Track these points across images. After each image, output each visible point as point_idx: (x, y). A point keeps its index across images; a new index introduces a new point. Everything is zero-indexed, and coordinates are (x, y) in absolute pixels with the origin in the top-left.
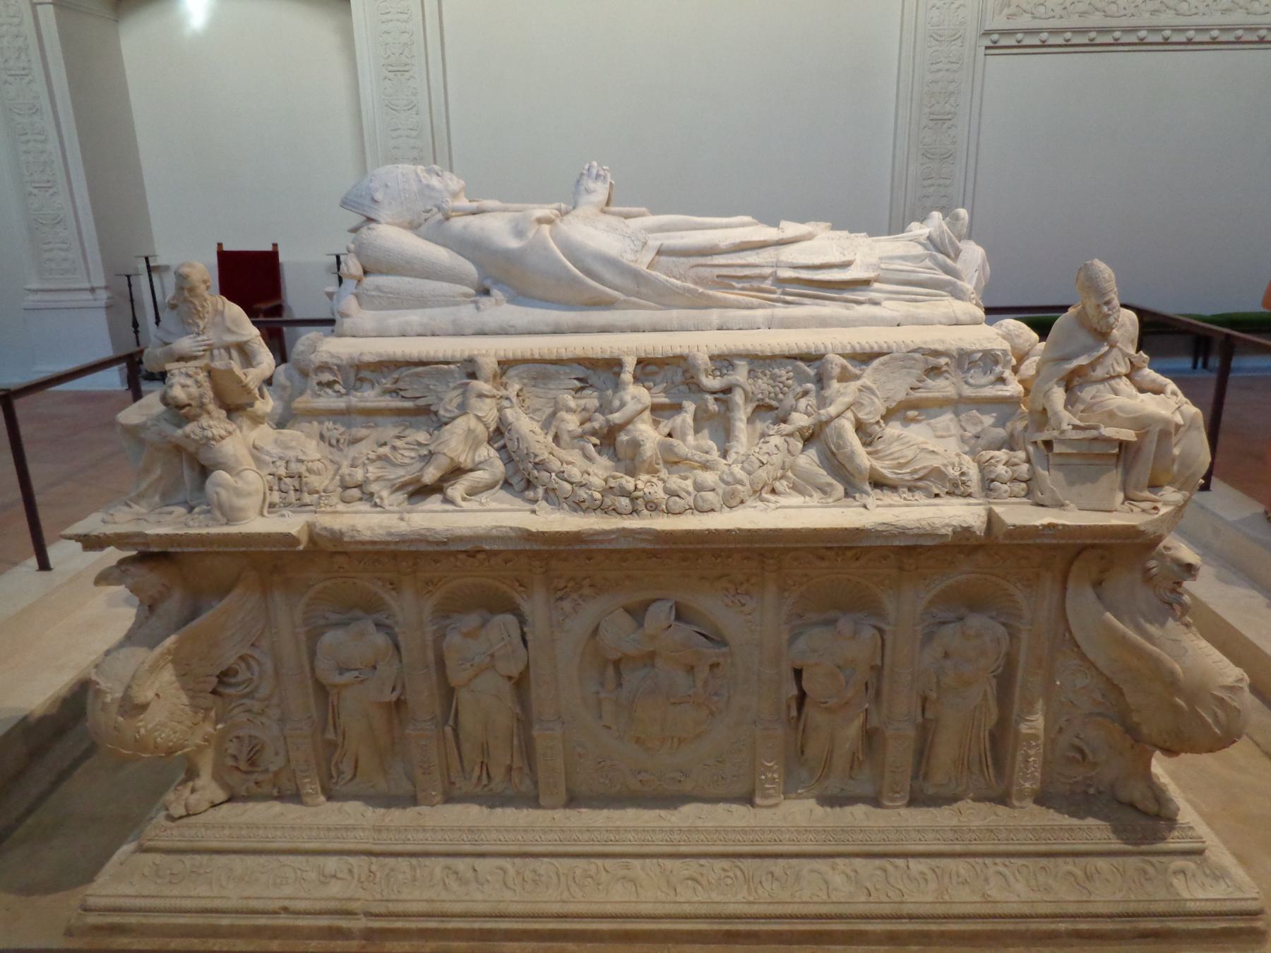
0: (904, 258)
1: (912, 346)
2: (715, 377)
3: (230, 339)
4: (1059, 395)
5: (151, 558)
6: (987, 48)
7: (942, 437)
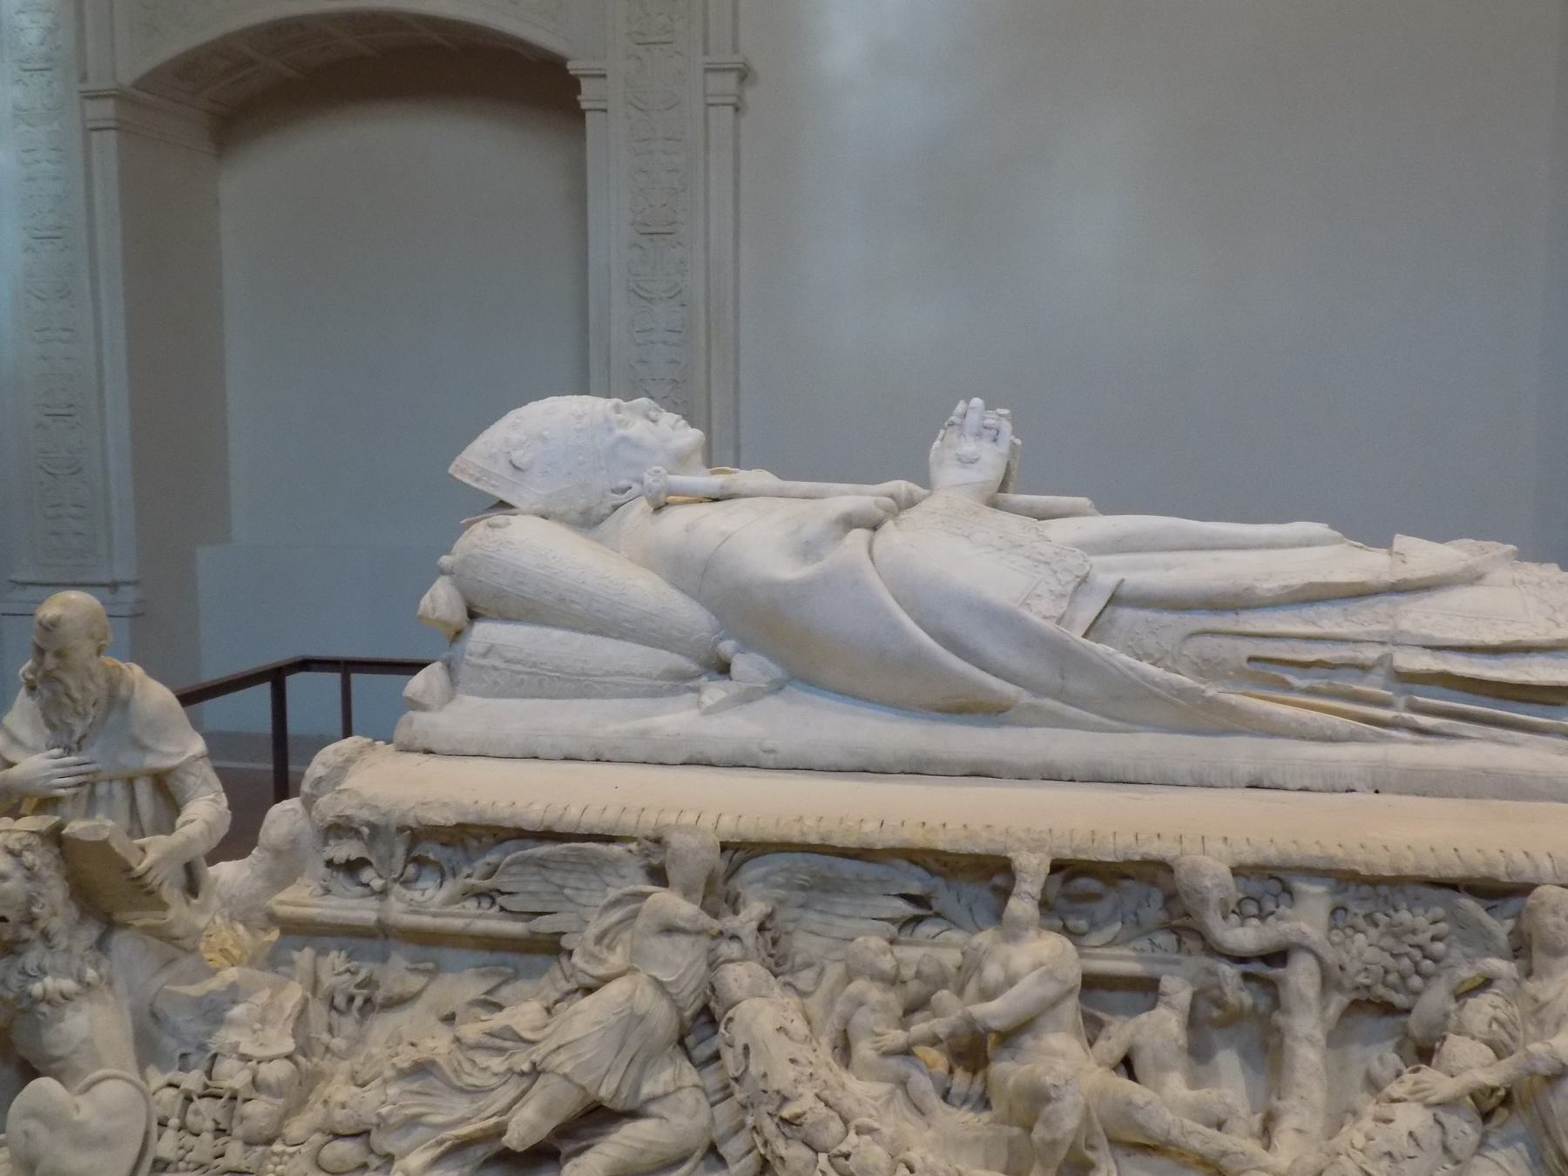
2: (1244, 918)
3: (130, 760)
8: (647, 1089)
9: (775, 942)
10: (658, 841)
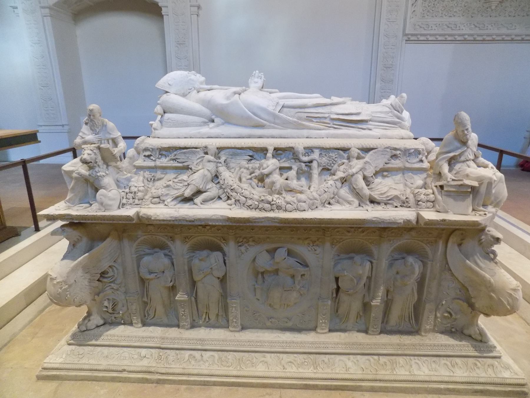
0: (381, 112)
2: (305, 156)
3: (108, 136)
4: (445, 168)
5: (74, 224)
6: (406, 41)
7: (397, 183)
8: (207, 188)
10: (206, 147)
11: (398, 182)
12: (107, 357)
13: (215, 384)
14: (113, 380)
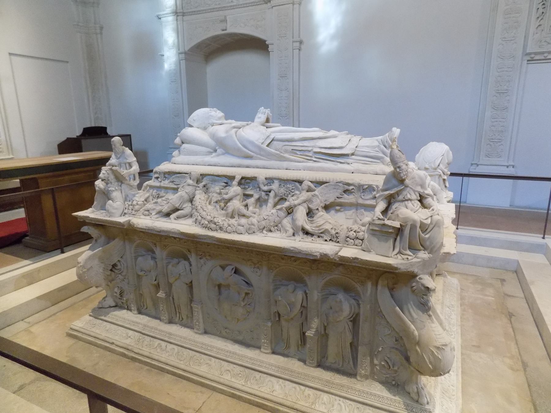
0: (368, 147)
1: (339, 180)
3: (125, 161)
6: (528, 61)
8: (184, 206)
9: (207, 189)
11: (349, 217)
12: (107, 330)
13: (169, 372)
14: (106, 348)
